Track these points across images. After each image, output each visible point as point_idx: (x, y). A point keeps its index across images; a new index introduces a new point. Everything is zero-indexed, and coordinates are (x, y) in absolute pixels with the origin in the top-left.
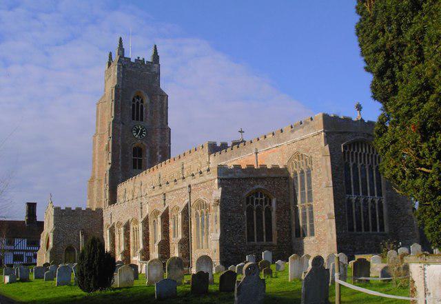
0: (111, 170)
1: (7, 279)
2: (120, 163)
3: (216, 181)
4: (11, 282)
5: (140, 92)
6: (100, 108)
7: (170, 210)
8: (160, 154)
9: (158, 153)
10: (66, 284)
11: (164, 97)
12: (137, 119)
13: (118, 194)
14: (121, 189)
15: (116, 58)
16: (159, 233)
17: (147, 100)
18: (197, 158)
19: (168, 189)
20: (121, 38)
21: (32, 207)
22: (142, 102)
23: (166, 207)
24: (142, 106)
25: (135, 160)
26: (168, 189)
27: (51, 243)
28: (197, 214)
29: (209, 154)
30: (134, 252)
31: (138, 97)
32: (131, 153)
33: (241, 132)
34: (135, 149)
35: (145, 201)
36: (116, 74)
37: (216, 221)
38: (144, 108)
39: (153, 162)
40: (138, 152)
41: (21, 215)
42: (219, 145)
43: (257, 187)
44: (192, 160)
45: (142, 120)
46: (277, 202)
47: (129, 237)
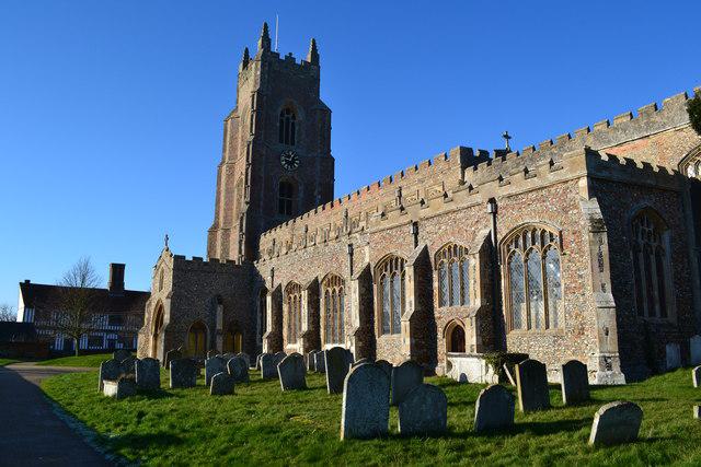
0: (249, 211)
1: (110, 389)
2: (262, 203)
3: (584, 182)
4: (121, 395)
5: (291, 103)
6: (229, 126)
7: (432, 255)
8: (320, 193)
9: (315, 193)
10: (373, 435)
11: (326, 112)
12: (293, 144)
13: (261, 248)
14: (265, 241)
15: (257, 50)
16: (410, 297)
17: (300, 116)
18: (436, 175)
19: (424, 212)
20: (266, 24)
21: (118, 271)
22: (294, 117)
23: (421, 246)
24: (293, 124)
25: (281, 201)
26: (424, 212)
27: (167, 318)
28: (327, 292)
29: (463, 169)
30: (326, 334)
31: (288, 111)
32: (277, 189)
33: (507, 137)
34: (282, 184)
35: (357, 239)
36: (259, 73)
37: (601, 265)
38: (297, 128)
39: (310, 204)
40: (287, 189)
41: (103, 281)
42: (477, 154)
43: (643, 204)
44: (421, 181)
45: (293, 144)
46: (672, 240)
47: (318, 309)
